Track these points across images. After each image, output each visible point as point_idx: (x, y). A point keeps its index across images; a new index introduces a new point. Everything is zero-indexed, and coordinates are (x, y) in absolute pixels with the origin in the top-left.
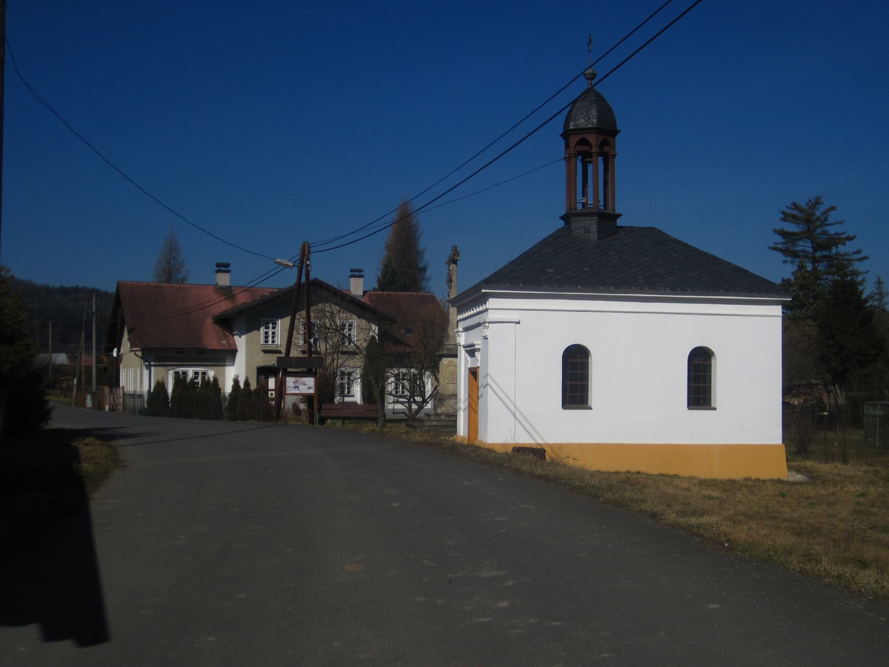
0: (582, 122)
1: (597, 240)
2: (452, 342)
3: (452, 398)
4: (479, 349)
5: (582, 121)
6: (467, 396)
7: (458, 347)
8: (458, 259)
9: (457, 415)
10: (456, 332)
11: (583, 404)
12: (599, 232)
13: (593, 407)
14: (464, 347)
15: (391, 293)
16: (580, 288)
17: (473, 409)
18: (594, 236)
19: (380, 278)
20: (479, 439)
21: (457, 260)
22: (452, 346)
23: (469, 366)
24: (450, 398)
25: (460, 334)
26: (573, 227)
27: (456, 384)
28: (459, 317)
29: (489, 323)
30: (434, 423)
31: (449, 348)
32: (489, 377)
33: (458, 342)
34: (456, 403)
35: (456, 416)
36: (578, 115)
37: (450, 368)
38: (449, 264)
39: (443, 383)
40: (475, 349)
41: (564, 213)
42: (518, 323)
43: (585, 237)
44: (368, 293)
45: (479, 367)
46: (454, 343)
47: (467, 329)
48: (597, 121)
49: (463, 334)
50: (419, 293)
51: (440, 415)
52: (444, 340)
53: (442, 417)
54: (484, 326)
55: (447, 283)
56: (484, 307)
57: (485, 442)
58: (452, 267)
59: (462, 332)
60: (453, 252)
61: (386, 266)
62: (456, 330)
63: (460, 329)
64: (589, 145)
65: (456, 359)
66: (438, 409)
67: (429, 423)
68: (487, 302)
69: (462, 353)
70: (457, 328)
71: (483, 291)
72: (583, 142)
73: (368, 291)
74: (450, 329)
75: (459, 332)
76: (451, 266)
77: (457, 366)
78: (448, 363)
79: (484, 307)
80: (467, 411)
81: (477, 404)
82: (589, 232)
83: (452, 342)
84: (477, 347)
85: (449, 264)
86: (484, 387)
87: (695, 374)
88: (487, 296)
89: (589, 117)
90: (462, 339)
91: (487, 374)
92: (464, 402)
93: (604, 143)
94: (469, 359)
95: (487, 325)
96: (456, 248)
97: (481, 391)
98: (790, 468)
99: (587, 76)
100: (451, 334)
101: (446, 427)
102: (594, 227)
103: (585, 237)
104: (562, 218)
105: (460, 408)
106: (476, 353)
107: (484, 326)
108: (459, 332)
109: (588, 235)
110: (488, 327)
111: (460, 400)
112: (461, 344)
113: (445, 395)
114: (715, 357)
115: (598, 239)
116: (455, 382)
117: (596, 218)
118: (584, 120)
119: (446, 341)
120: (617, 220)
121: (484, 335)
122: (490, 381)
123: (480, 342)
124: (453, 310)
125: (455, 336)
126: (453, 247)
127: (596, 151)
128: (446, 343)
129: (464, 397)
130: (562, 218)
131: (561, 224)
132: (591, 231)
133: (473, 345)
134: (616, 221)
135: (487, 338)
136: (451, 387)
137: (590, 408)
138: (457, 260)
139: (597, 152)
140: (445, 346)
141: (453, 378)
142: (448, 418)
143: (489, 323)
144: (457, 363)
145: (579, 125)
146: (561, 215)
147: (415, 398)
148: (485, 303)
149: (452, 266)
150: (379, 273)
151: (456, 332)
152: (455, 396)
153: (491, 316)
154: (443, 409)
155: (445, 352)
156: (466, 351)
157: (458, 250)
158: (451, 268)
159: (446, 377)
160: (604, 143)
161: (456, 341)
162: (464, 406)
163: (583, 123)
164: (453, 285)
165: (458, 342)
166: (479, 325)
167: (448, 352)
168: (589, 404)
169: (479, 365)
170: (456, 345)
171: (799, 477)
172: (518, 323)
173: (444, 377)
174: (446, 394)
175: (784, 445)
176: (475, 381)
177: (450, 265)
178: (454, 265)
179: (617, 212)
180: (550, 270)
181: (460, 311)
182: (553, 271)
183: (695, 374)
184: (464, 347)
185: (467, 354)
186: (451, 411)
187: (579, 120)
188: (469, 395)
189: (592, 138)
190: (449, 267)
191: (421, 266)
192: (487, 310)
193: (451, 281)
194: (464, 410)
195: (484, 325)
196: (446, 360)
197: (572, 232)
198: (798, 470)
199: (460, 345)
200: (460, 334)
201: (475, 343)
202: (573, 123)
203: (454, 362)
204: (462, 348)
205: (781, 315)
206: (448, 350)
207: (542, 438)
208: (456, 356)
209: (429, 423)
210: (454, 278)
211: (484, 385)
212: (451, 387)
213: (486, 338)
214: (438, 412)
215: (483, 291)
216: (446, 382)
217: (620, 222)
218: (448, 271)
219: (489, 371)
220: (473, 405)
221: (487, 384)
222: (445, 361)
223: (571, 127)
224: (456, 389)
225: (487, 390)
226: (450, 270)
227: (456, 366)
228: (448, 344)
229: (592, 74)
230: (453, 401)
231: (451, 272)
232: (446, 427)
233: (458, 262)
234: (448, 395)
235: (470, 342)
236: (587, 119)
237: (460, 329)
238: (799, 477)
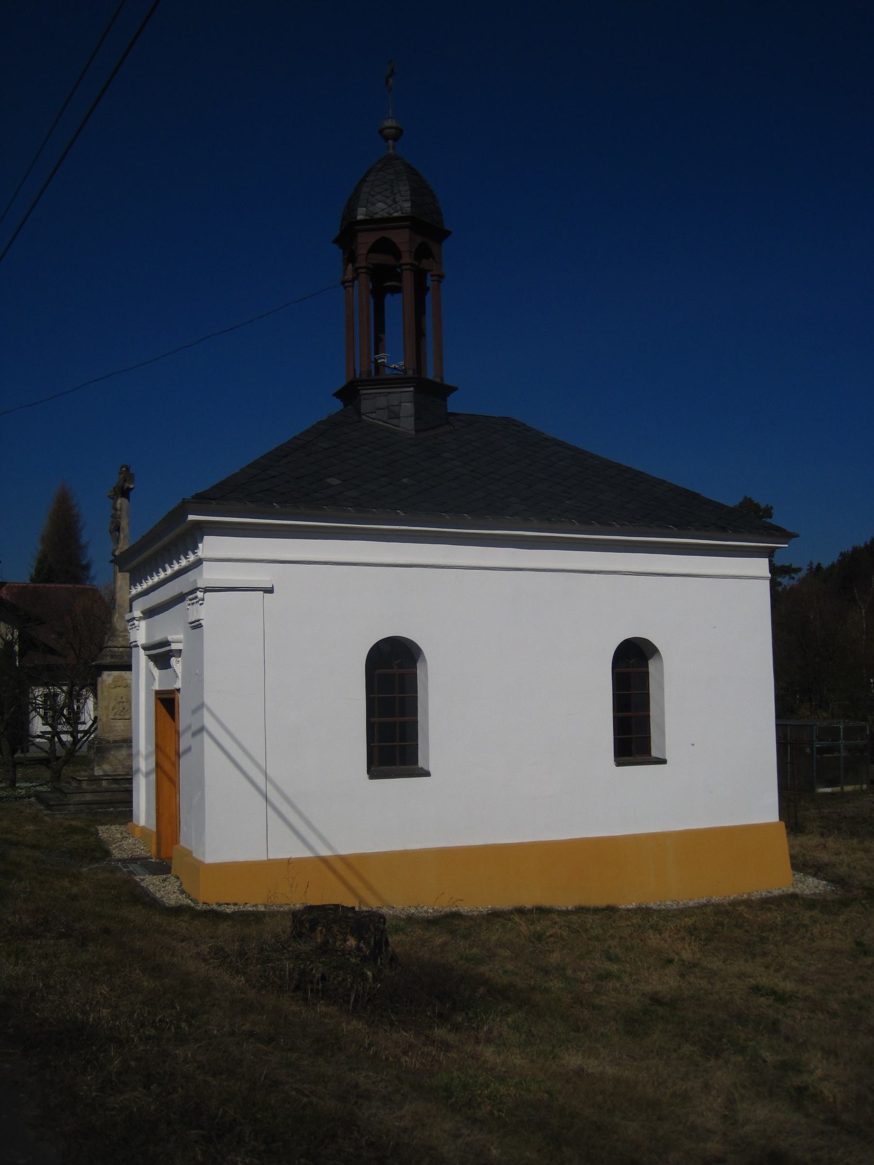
0: (381, 209)
1: (413, 433)
2: (121, 641)
3: (121, 747)
4: (180, 651)
5: (381, 205)
6: (152, 748)
7: (134, 649)
8: (131, 486)
9: (132, 779)
10: (129, 621)
11: (403, 762)
12: (418, 416)
13: (432, 770)
14: (146, 648)
15: (38, 585)
16: (402, 514)
17: (165, 773)
18: (407, 424)
19: (33, 576)
20: (181, 844)
21: (130, 490)
22: (121, 649)
23: (157, 687)
24: (119, 747)
25: (136, 623)
26: (366, 406)
27: (130, 719)
28: (134, 592)
29: (206, 590)
30: (89, 797)
31: (115, 652)
32: (206, 712)
33: (132, 640)
34: (130, 756)
35: (130, 781)
36: (373, 196)
37: (117, 690)
38: (114, 498)
39: (104, 719)
40: (171, 651)
41: (342, 383)
42: (270, 591)
43: (389, 425)
44: (7, 585)
45: (178, 690)
46: (124, 643)
47: (149, 614)
48: (411, 206)
49: (143, 624)
50: (77, 586)
51: (98, 779)
52: (106, 638)
53: (104, 783)
54: (191, 600)
55: (110, 532)
56: (192, 558)
57: (200, 858)
58: (121, 504)
59: (140, 619)
60: (122, 475)
61: (41, 562)
62: (128, 616)
63: (137, 613)
64: (398, 255)
65: (128, 672)
66: (96, 768)
67: (77, 798)
68: (200, 545)
69: (141, 660)
70: (131, 611)
71: (191, 517)
72: (384, 246)
73: (7, 583)
74: (116, 617)
75: (134, 619)
76: (119, 501)
77: (130, 687)
78: (114, 681)
79: (192, 558)
80: (153, 777)
81: (176, 765)
82: (398, 417)
83: (121, 641)
84: (174, 646)
85: (114, 498)
86: (194, 734)
87: (618, 692)
88: (201, 531)
89: (395, 198)
90: (141, 634)
91: (201, 706)
92: (147, 757)
93: (423, 252)
94: (156, 672)
95: (200, 594)
96: (128, 469)
97: (185, 741)
98: (800, 865)
99: (386, 131)
100: (118, 627)
101: (111, 803)
102: (408, 408)
103: (389, 425)
104: (338, 395)
105: (138, 770)
106: (173, 660)
107: (191, 600)
108: (134, 619)
109: (394, 421)
110: (203, 600)
111: (138, 753)
112: (139, 644)
113: (108, 742)
114: (425, 660)
115: (417, 431)
116: (127, 717)
117: (412, 389)
118: (385, 203)
119: (109, 640)
120: (448, 398)
121: (190, 621)
122: (208, 722)
123: (181, 637)
124: (122, 579)
125: (126, 631)
126: (122, 467)
127: (409, 261)
128: (110, 644)
129: (146, 748)
130: (338, 395)
131: (338, 405)
132: (401, 415)
133: (167, 643)
134: (446, 400)
135: (200, 626)
136: (120, 725)
137: (427, 774)
138: (130, 490)
139: (411, 264)
140: (108, 649)
141: (124, 709)
142: (115, 786)
143: (206, 590)
144: (131, 680)
145: (376, 213)
146: (336, 389)
147: (62, 736)
148: (194, 548)
149: (121, 502)
150: (33, 571)
151: (129, 621)
152: (127, 742)
153: (209, 575)
154: (106, 767)
155: (108, 660)
156: (150, 657)
157: (131, 472)
158: (118, 506)
159: (110, 708)
160: (423, 252)
161: (129, 640)
162: (146, 765)
163: (383, 210)
164: (122, 536)
165: (132, 640)
166: (180, 598)
167: (112, 660)
168: (421, 764)
169: (178, 685)
170: (130, 647)
171: (812, 886)
172: (270, 591)
173: (107, 708)
174: (111, 739)
175: (783, 824)
176: (173, 722)
177: (117, 500)
178: (125, 500)
179: (447, 382)
180: (334, 481)
181: (135, 580)
182: (340, 482)
183: (618, 692)
184: (146, 648)
185: (151, 664)
186: (121, 771)
187: (373, 204)
188: (157, 746)
189: (401, 238)
190: (115, 502)
191: (84, 562)
192: (199, 562)
193: (118, 529)
194: (147, 775)
195: (191, 597)
196: (109, 675)
197: (363, 417)
198: (816, 869)
199: (137, 646)
200: (136, 623)
201: (170, 638)
202: (364, 209)
203: (126, 679)
204: (142, 652)
205: (769, 575)
206: (112, 656)
207: (329, 847)
208: (128, 667)
209: (77, 798)
210: (124, 523)
211: (195, 728)
212: (120, 725)
213: (197, 625)
214: (96, 774)
215: (191, 517)
216: (111, 717)
217: (454, 404)
218: (113, 512)
219: (208, 699)
220: (167, 766)
221: (202, 729)
222: (108, 677)
223: (359, 217)
224: (129, 729)
225: (203, 738)
226: (116, 509)
227: (128, 686)
228: (115, 644)
229: (397, 128)
230: (124, 752)
231: (118, 512)
232: (111, 803)
233: (131, 494)
234: (115, 742)
235: (158, 638)
236: (390, 202)
237: (137, 613)
238: (812, 886)
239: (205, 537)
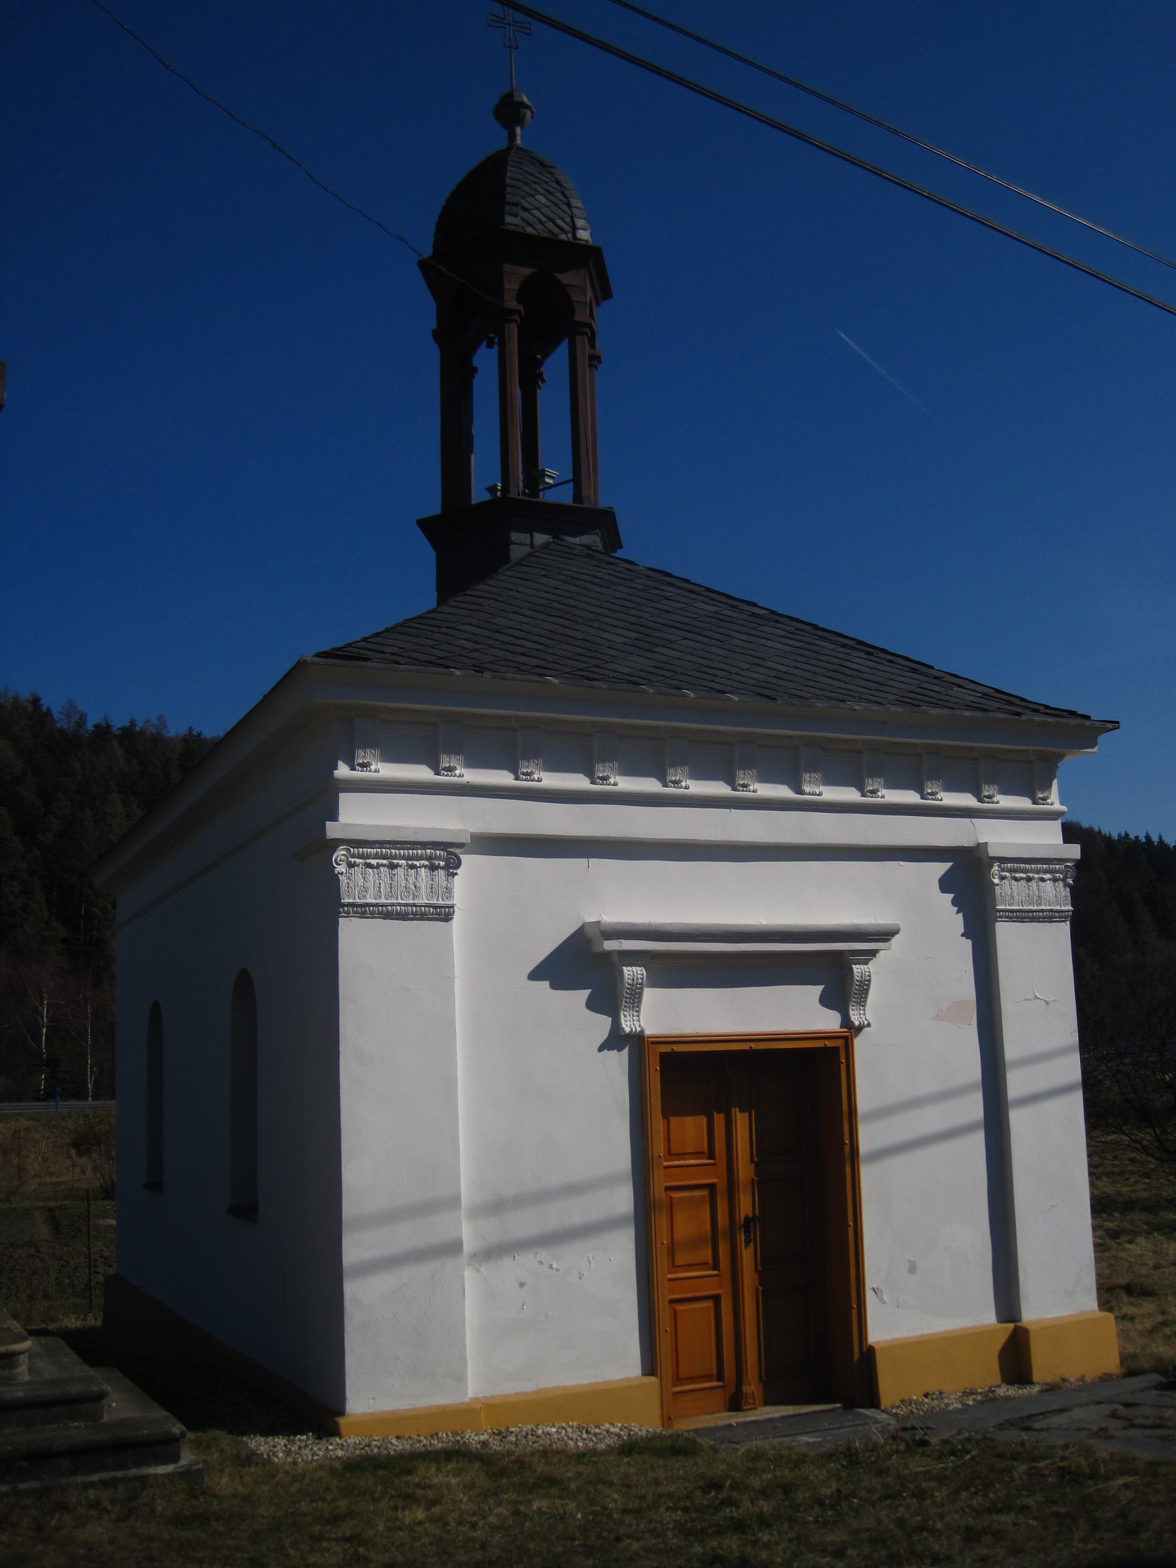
239: (328, 823)
